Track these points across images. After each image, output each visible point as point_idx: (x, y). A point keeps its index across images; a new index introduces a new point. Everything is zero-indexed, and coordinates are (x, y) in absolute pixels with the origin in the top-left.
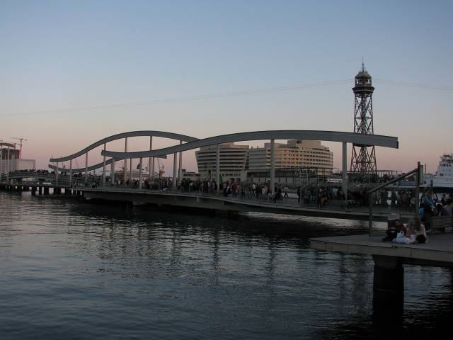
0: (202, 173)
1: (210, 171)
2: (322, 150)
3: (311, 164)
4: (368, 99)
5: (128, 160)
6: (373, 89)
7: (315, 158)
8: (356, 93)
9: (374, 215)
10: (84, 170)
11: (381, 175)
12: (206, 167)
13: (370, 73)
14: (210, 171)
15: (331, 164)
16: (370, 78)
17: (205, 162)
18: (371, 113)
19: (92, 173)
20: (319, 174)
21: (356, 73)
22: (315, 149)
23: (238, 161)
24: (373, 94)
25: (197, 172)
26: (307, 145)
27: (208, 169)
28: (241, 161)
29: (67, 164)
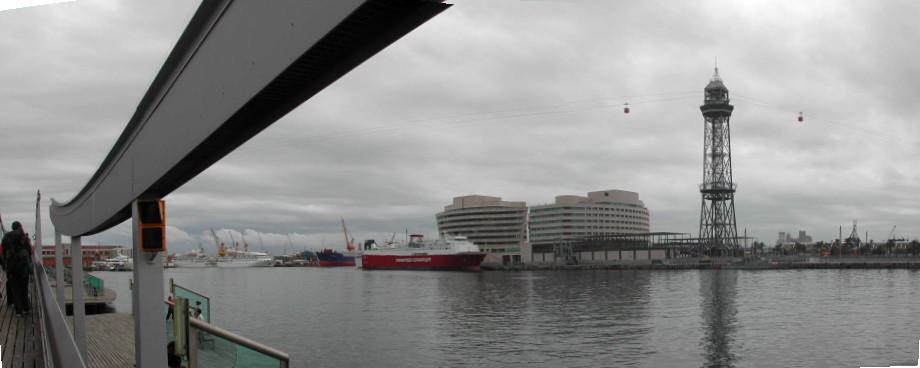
6: (731, 108)
8: (705, 115)
13: (726, 85)
16: (727, 92)
21: (705, 84)
23: (455, 224)
24: (731, 118)
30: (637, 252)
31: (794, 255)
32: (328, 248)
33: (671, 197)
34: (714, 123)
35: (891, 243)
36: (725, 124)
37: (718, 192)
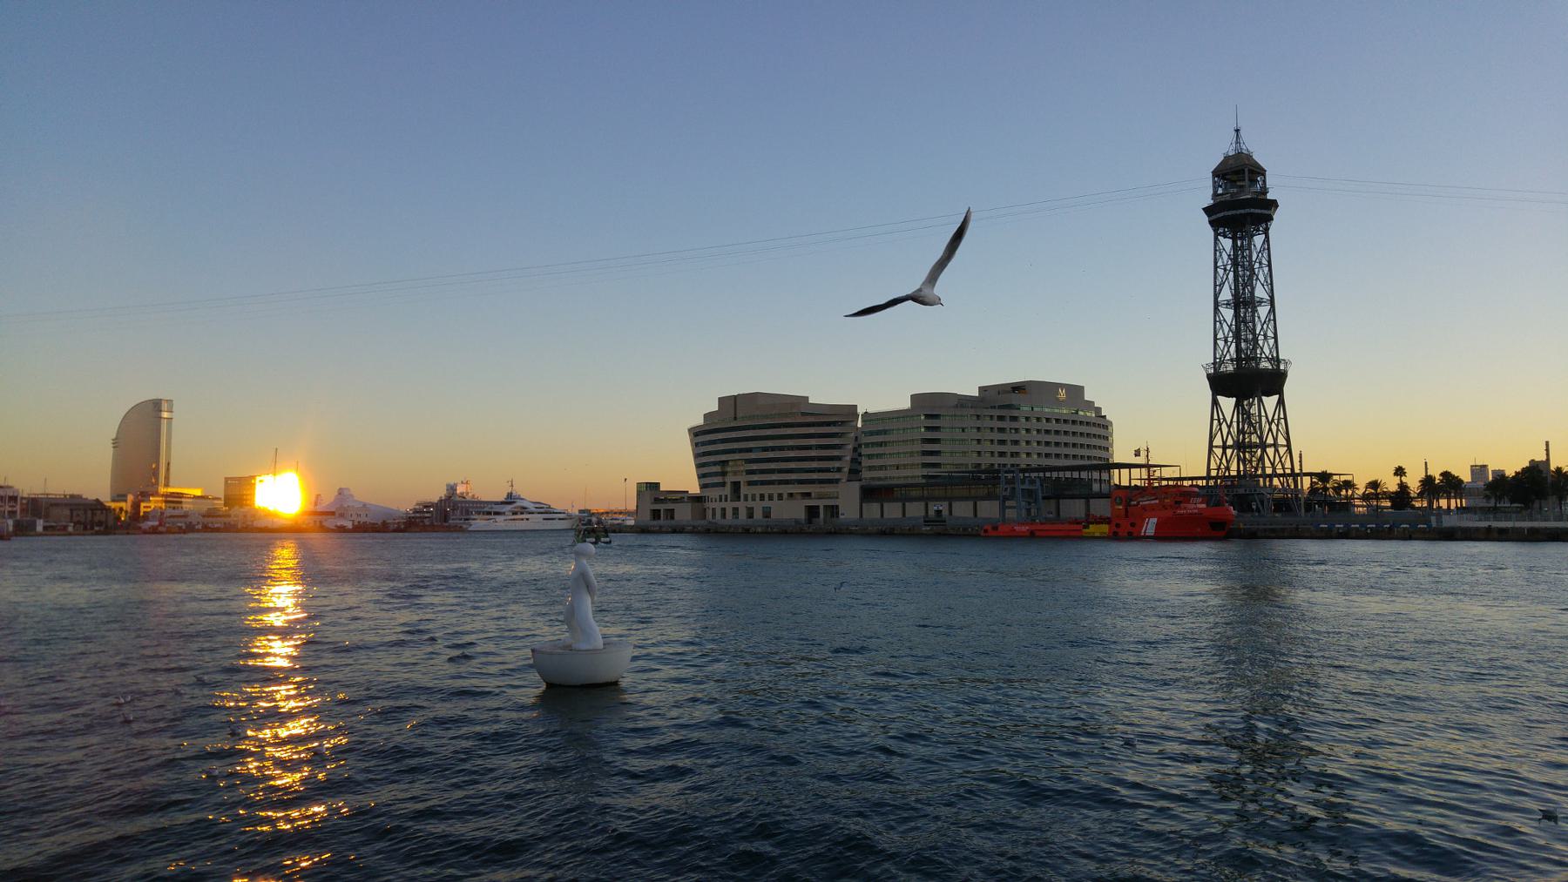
0: (713, 493)
1: (736, 485)
6: (1274, 204)
12: (724, 474)
13: (1260, 158)
14: (736, 485)
16: (1262, 172)
17: (723, 457)
24: (1274, 227)
25: (694, 488)
27: (730, 479)
28: (836, 453)
30: (1092, 501)
31: (1413, 513)
32: (76, 492)
33: (1164, 427)
34: (1234, 239)
35: (511, 499)
36: (1258, 240)
37: (1247, 379)
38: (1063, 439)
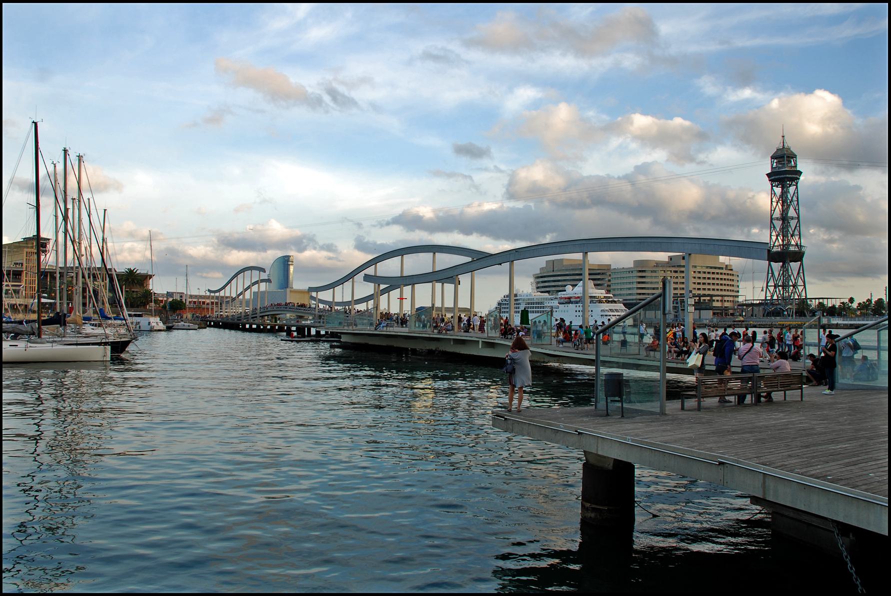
2: (719, 268)
3: (704, 289)
4: (792, 189)
5: (407, 290)
6: (800, 173)
7: (711, 281)
9: (602, 358)
10: (349, 303)
11: (814, 304)
15: (735, 289)
18: (797, 211)
19: (825, 303)
20: (715, 304)
22: (711, 268)
23: (546, 284)
26: (700, 261)
29: (326, 296)
38: (716, 282)
